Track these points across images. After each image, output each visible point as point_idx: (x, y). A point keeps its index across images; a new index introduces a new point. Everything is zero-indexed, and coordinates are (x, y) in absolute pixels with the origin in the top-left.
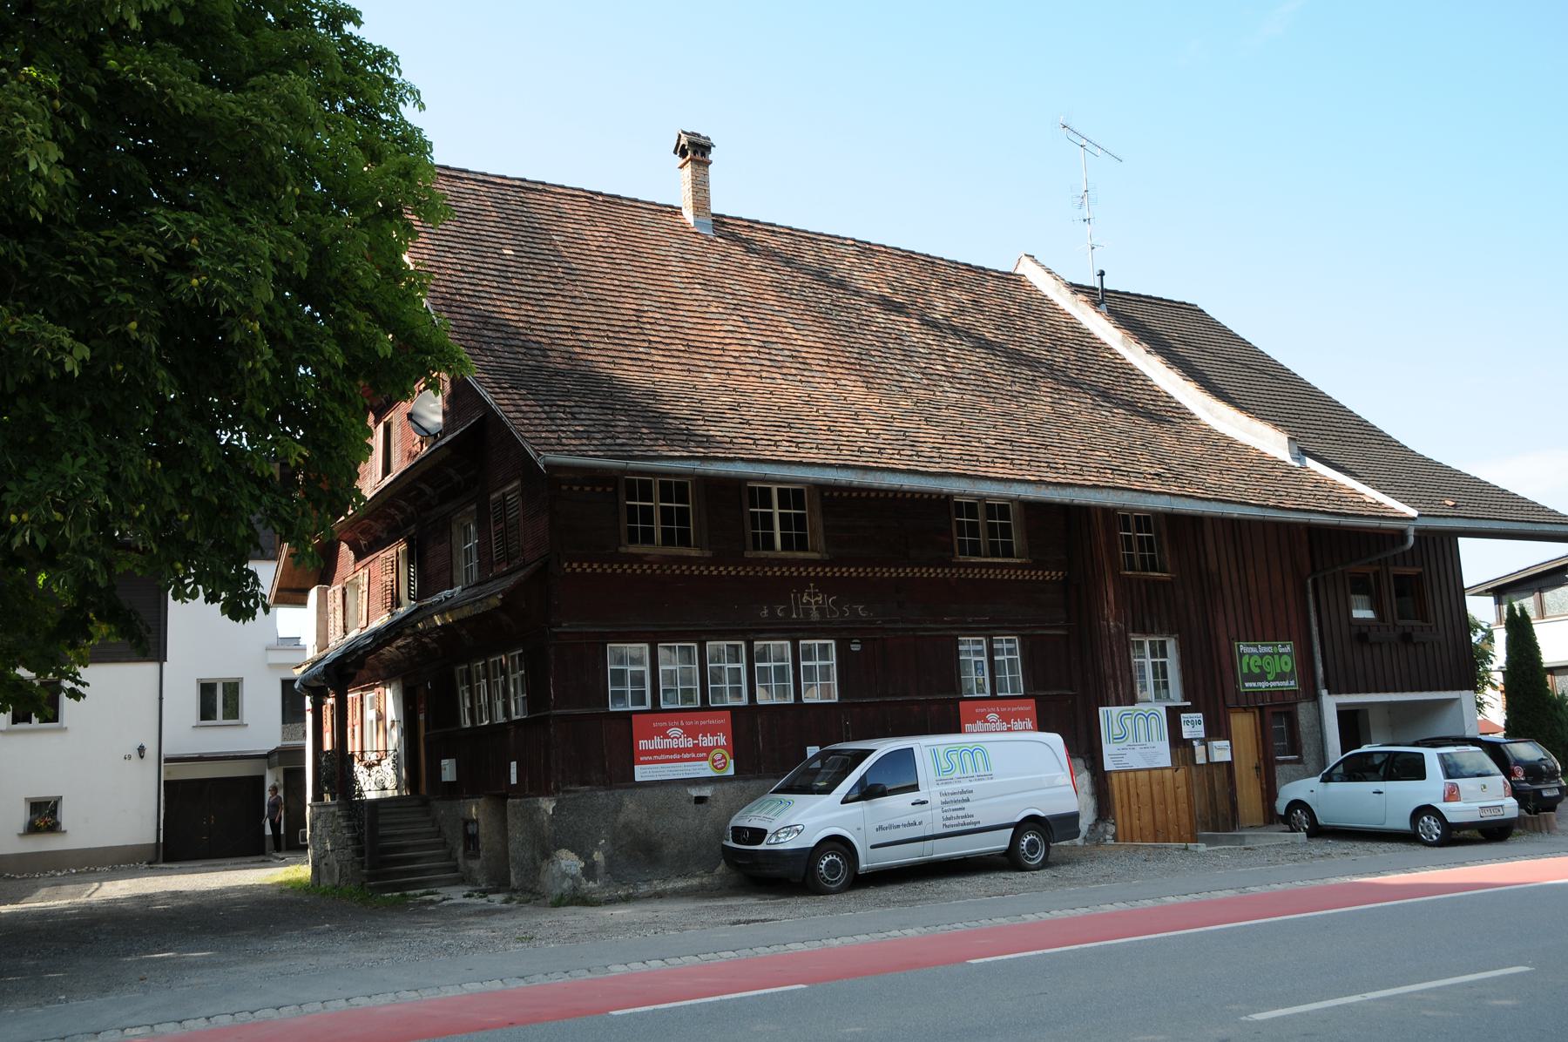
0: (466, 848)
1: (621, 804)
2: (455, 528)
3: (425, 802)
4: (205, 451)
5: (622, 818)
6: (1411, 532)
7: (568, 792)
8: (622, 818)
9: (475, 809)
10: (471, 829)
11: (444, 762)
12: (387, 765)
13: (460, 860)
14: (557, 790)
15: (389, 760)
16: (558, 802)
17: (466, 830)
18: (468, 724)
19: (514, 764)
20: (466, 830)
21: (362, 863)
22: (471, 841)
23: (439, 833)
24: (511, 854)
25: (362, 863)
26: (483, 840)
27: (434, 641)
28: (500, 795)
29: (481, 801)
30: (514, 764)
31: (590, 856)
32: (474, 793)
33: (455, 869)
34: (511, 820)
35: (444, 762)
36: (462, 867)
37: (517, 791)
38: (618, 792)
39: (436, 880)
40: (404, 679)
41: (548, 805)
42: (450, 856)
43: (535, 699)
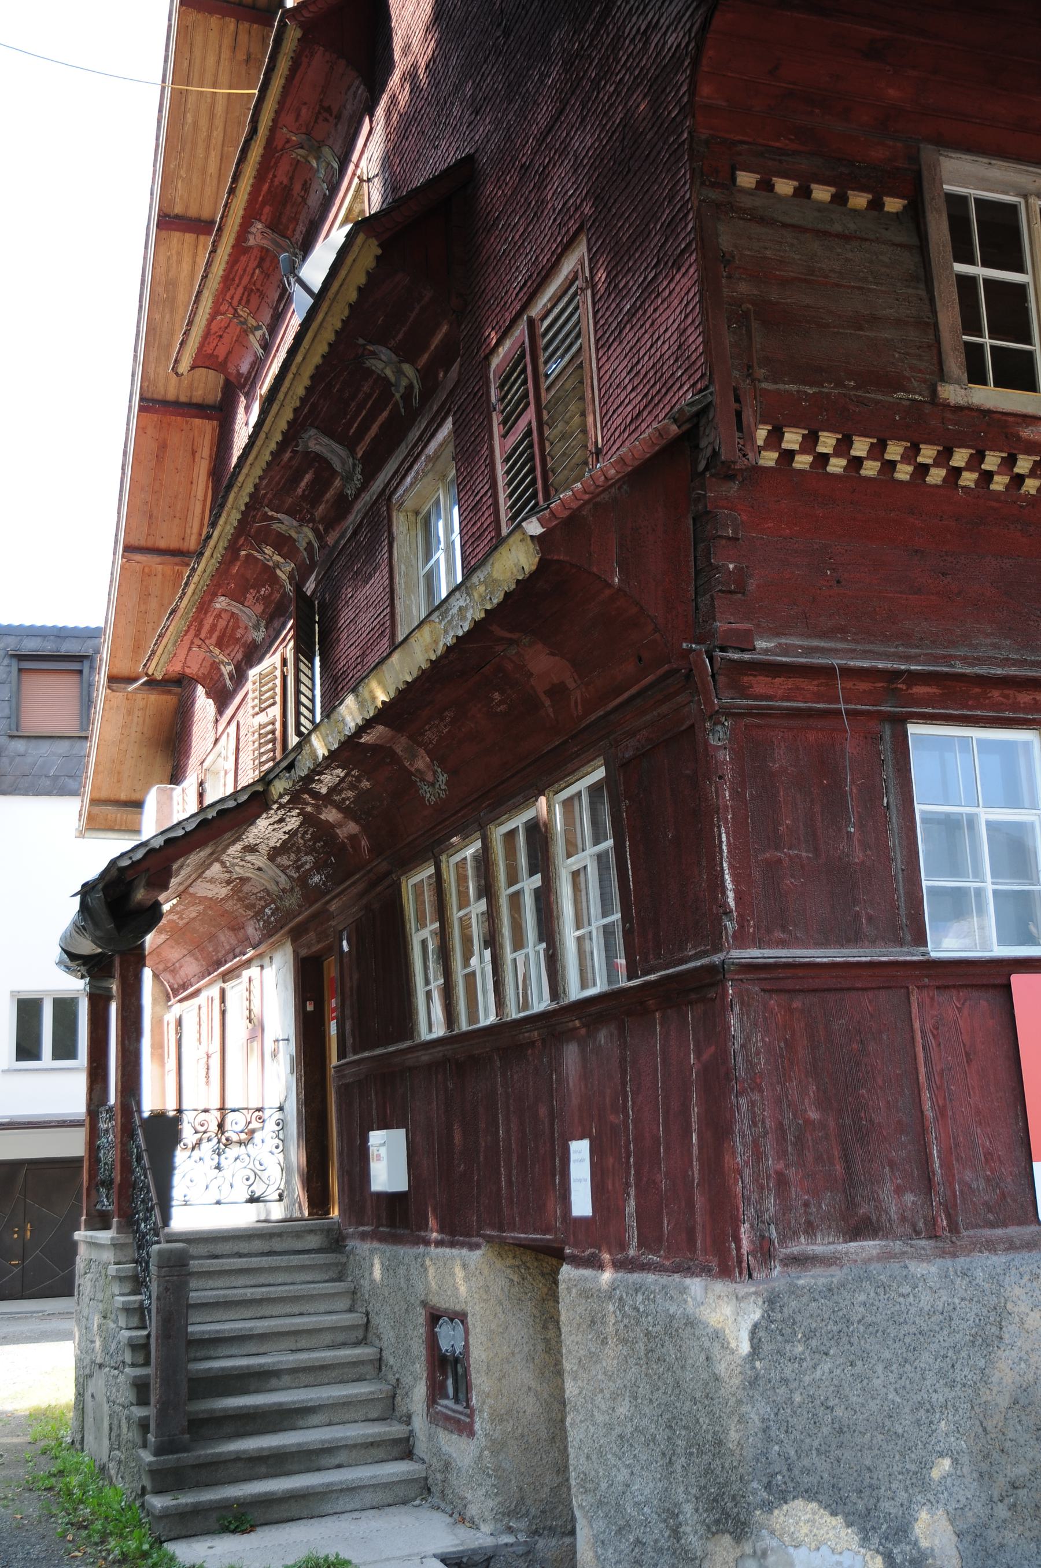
0: (436, 1391)
1: (1000, 1314)
2: (400, 525)
3: (336, 1242)
4: (667, 1263)
5: (1006, 1372)
6: (83, 1227)
7: (800, 1261)
8: (1006, 1372)
9: (462, 1276)
10: (449, 1338)
11: (376, 1137)
12: (267, 1136)
13: (420, 1423)
14: (765, 1252)
15: (271, 1126)
16: (772, 1302)
17: (432, 1342)
18: (439, 1031)
19: (580, 1151)
20: (432, 1342)
21: (144, 1426)
22: (448, 1371)
23: (365, 1333)
24: (577, 1461)
25: (144, 1426)
26: (481, 1382)
27: (348, 813)
28: (544, 1252)
29: (476, 1257)
30: (580, 1151)
31: (901, 1531)
32: (458, 1232)
33: (404, 1449)
34: (574, 1342)
35: (376, 1137)
36: (421, 1448)
37: (594, 1240)
38: (984, 1265)
39: (351, 1489)
40: (296, 935)
41: (726, 1314)
42: (390, 1407)
43: (659, 897)
